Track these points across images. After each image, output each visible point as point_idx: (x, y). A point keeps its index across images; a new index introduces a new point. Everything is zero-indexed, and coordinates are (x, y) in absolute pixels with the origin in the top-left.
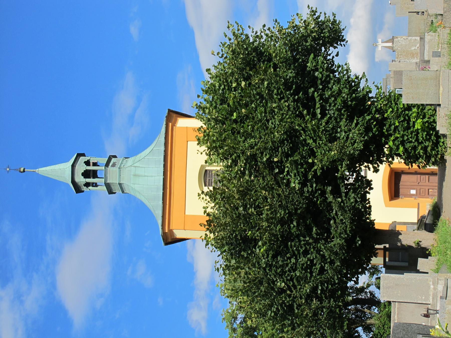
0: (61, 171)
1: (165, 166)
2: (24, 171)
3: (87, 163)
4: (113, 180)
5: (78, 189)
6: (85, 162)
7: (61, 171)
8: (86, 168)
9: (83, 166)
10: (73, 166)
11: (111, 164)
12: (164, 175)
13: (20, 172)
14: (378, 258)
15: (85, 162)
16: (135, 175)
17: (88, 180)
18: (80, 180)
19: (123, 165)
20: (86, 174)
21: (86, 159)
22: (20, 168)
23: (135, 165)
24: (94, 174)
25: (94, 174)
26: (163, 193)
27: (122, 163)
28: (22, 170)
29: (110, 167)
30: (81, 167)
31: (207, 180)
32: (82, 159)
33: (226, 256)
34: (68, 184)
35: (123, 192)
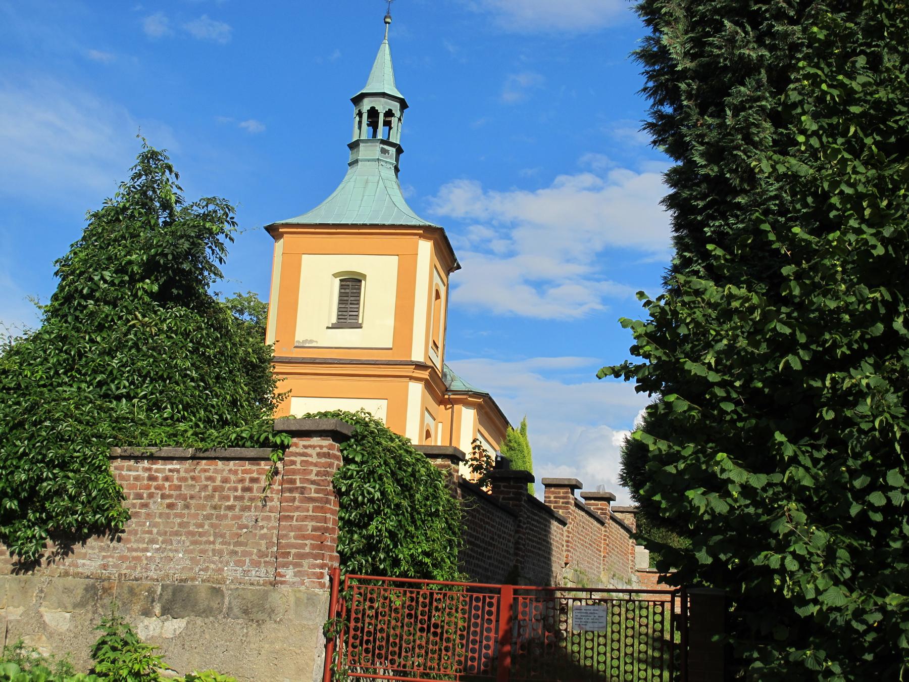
0: (383, 78)
1: (364, 226)
2: (386, 23)
3: (389, 114)
4: (364, 151)
5: (357, 100)
6: (390, 110)
7: (383, 78)
8: (382, 110)
9: (384, 108)
10: (384, 95)
11: (386, 147)
12: (352, 224)
13: (386, 17)
14: (643, 176)
15: (390, 110)
16: (367, 182)
17: (365, 116)
18: (366, 105)
19: (384, 164)
20: (373, 113)
21: (397, 113)
22: (390, 17)
23: (381, 181)
24: (373, 124)
25: (373, 124)
26: (347, 225)
27: (386, 162)
28: (388, 20)
29: (382, 146)
30: (382, 106)
31: (348, 283)
32: (395, 107)
33: (234, 344)
34: (363, 87)
35: (350, 165)
